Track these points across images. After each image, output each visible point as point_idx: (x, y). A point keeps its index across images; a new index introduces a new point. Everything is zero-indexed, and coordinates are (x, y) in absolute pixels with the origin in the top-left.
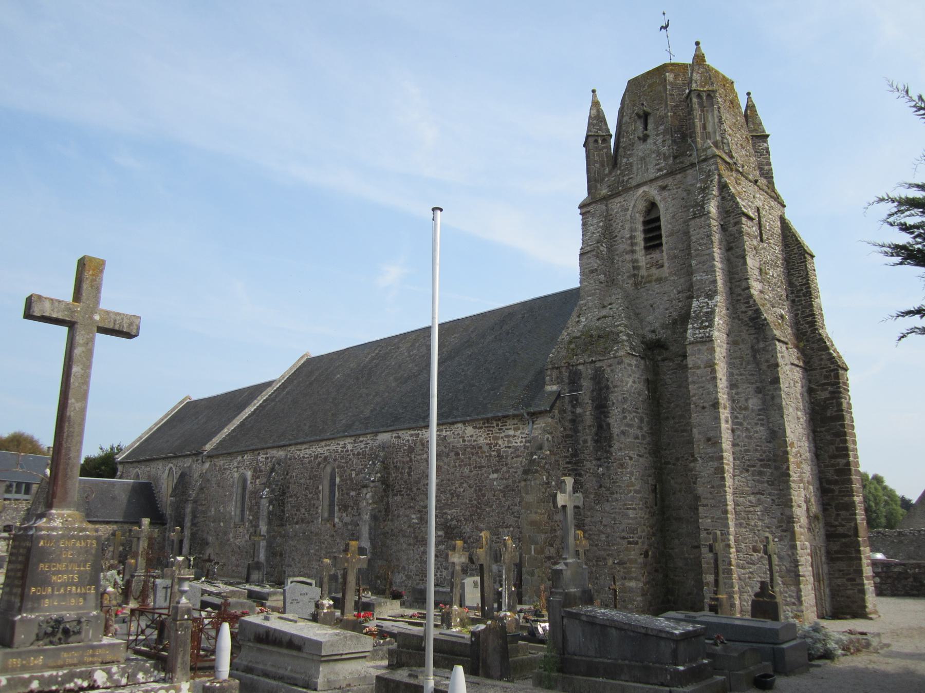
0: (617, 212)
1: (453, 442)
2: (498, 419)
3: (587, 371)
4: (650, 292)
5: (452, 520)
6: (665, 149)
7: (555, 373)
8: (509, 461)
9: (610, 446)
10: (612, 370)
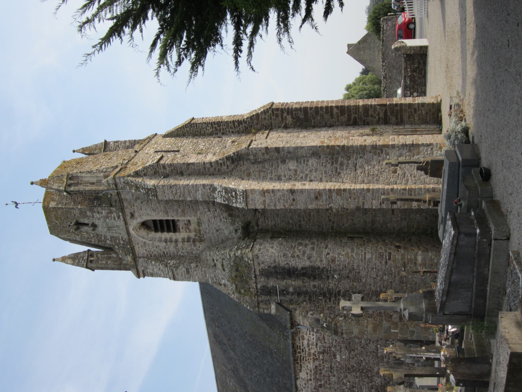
0: (146, 250)
1: (311, 389)
2: (295, 352)
3: (262, 281)
7: (262, 306)
8: (327, 345)
9: (319, 268)
10: (263, 263)
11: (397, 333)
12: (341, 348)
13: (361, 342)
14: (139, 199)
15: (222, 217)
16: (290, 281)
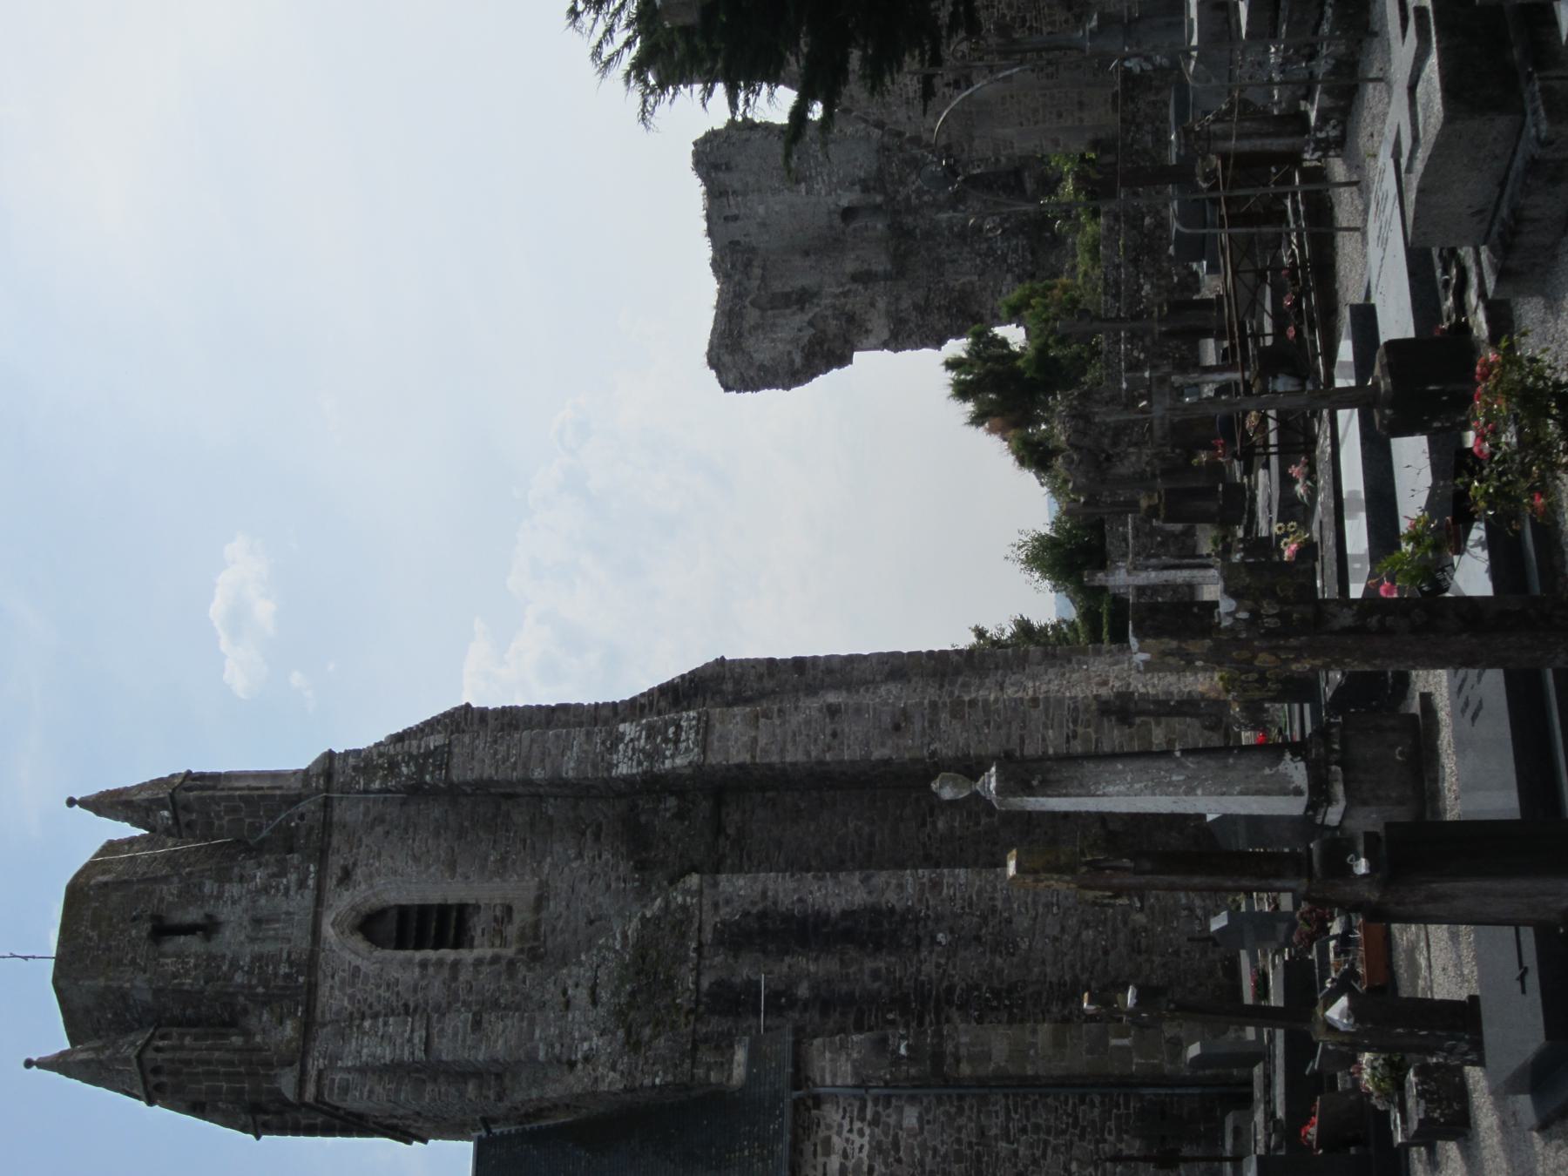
0: (352, 998)
4: (561, 924)
7: (706, 1056)
9: (892, 910)
10: (728, 902)
13: (1016, 1153)
14: (383, 821)
15: (613, 875)
16: (803, 961)
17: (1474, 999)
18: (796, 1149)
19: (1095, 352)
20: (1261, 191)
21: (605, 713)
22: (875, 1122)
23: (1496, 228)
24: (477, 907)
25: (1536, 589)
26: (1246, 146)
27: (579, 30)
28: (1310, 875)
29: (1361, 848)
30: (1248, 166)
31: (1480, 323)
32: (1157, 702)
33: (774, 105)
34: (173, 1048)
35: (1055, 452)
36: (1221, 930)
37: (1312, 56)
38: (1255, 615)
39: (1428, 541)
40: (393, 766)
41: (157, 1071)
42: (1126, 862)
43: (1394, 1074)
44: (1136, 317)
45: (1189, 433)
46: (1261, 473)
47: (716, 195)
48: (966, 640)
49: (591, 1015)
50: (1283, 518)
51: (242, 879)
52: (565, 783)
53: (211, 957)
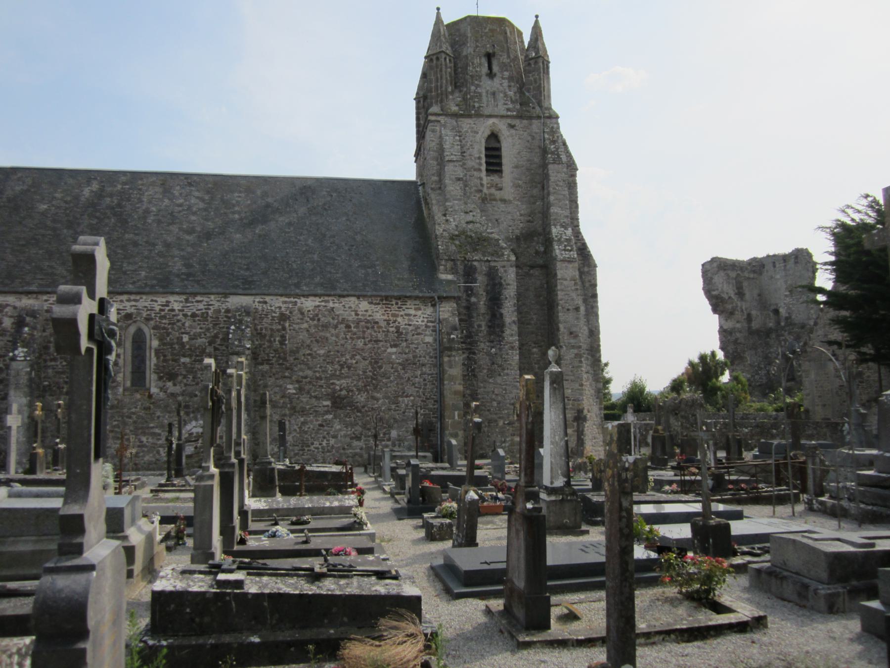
0: (467, 132)
1: (342, 315)
2: (399, 298)
3: (481, 268)
5: (341, 390)
6: (511, 93)
7: (449, 265)
8: (409, 337)
9: (503, 332)
10: (505, 271)
11: (454, 418)
12: (406, 354)
17: (477, 545)
18: (417, 298)
19: (719, 410)
20: (790, 476)
21: (575, 223)
22: (427, 326)
23: (778, 570)
24: (501, 177)
25: (636, 576)
26: (810, 472)
27: (859, 199)
28: (526, 487)
29: (536, 506)
30: (801, 472)
31: (738, 560)
32: (583, 431)
33: (825, 280)
34: (446, 65)
35: (679, 394)
36: (498, 453)
37: (850, 500)
38: (627, 470)
39: (650, 536)
40: (554, 142)
41: (438, 59)
42: (530, 419)
43: (450, 515)
44: (735, 426)
45: (690, 447)
46: (672, 473)
47: (785, 258)
48: (604, 360)
49: (463, 222)
50: (655, 481)
51: (510, 86)
52: (548, 208)
53: (480, 77)
